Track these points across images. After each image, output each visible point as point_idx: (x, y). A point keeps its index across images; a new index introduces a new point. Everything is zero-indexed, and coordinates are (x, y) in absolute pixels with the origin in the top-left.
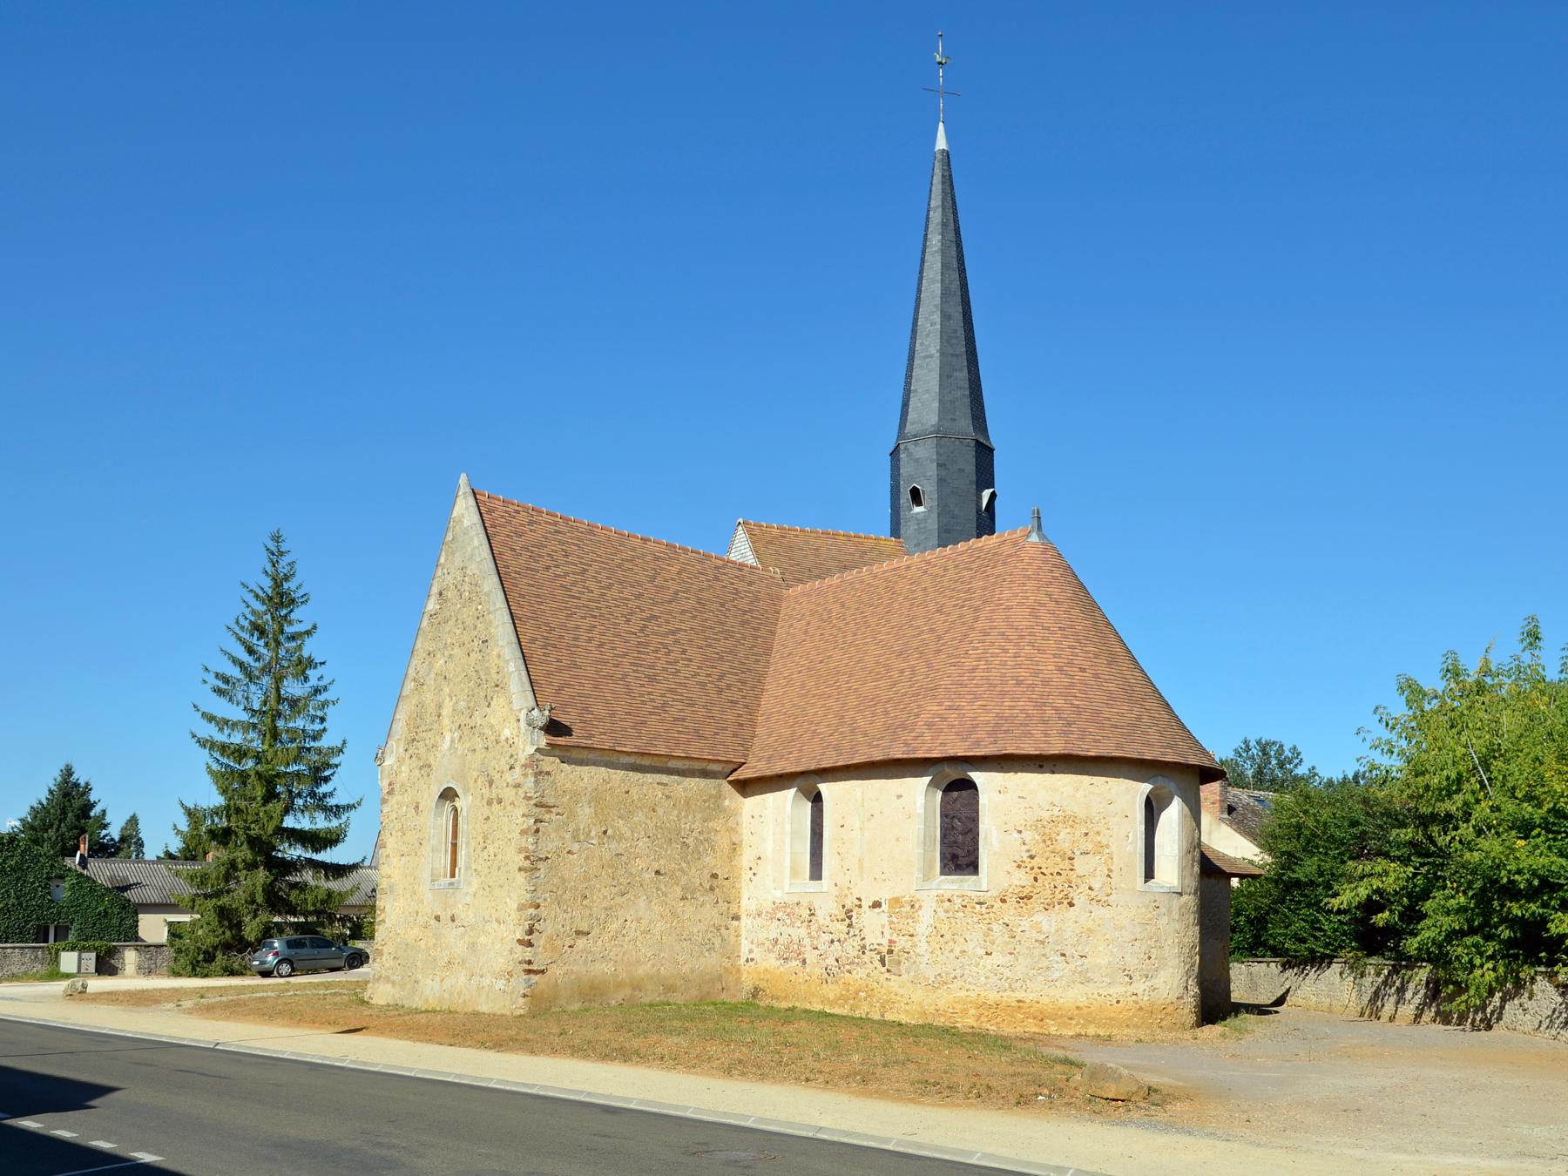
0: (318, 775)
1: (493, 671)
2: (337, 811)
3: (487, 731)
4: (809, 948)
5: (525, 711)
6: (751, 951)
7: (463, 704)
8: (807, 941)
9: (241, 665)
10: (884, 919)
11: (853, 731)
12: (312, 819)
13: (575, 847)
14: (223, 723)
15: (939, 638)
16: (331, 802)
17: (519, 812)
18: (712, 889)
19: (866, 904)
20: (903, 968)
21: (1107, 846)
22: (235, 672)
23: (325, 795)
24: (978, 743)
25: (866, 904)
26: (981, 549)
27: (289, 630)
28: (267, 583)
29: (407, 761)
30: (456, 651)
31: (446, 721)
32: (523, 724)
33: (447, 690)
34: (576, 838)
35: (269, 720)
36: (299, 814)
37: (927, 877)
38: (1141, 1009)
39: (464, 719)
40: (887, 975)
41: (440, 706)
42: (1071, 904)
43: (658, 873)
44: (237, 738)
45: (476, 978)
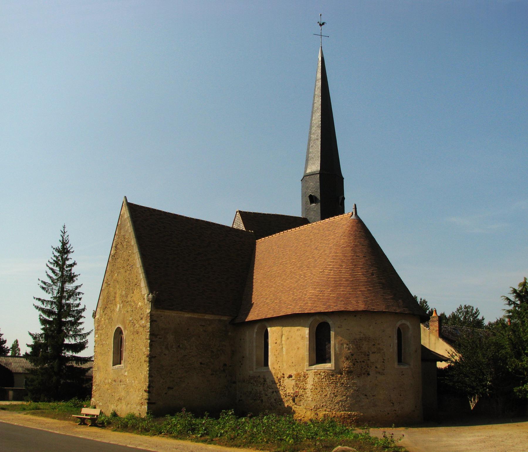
0: (75, 323)
1: (134, 278)
2: (84, 336)
3: (133, 304)
4: (264, 395)
5: (146, 295)
6: (241, 396)
7: (124, 292)
8: (263, 392)
9: (50, 277)
10: (293, 382)
11: (280, 302)
12: (75, 339)
13: (167, 352)
14: (43, 301)
15: (316, 260)
16: (83, 332)
17: (144, 337)
18: (224, 370)
19: (286, 376)
20: (302, 403)
21: (383, 350)
22: (49, 281)
23: (80, 329)
24: (329, 306)
25: (286, 376)
26: (333, 222)
27: (68, 263)
28: (60, 245)
29: (104, 316)
30: (121, 270)
31: (118, 299)
32: (146, 300)
33: (118, 286)
34: (167, 348)
35: (59, 301)
36: (70, 338)
37: (311, 365)
38: (397, 416)
39: (124, 299)
40: (295, 406)
41: (115, 293)
42: (369, 374)
43: (201, 363)
44: (49, 307)
45: (129, 405)
